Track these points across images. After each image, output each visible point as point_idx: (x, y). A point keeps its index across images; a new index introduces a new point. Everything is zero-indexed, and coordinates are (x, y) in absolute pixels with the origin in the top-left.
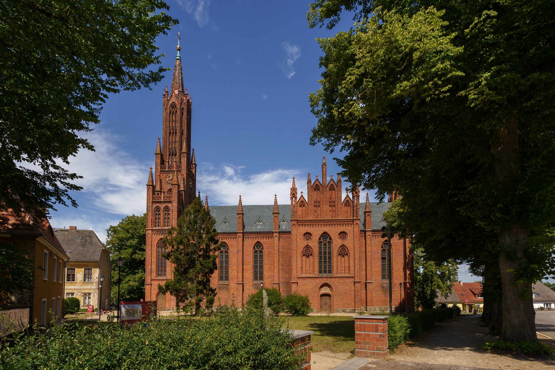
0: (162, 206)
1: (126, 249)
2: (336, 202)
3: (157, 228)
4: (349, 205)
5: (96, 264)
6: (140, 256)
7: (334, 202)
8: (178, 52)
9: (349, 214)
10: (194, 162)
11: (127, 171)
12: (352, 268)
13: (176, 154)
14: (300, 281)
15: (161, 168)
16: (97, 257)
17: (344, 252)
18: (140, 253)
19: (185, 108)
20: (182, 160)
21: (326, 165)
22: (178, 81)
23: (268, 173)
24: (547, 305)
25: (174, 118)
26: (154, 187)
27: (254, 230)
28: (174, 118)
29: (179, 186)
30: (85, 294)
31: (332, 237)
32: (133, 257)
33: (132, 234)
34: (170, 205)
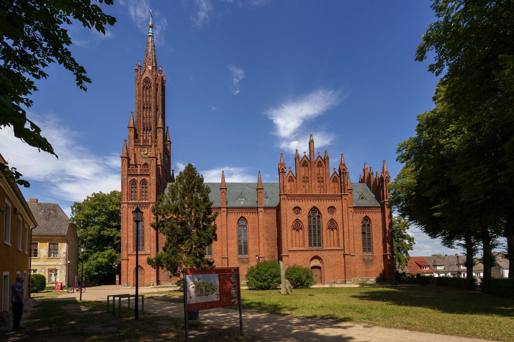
0: (139, 179)
1: (92, 226)
2: (324, 178)
3: (134, 201)
4: (337, 182)
5: (63, 239)
6: (109, 233)
7: (322, 178)
8: (151, 29)
9: (336, 190)
10: (168, 140)
11: (84, 164)
12: (341, 241)
13: (151, 129)
14: (291, 254)
15: (135, 142)
16: (64, 231)
17: (333, 226)
18: (109, 229)
19: (160, 84)
20: (158, 135)
21: (313, 143)
22: (151, 57)
23: (217, 169)
24: (477, 274)
25: (148, 93)
26: (129, 160)
27: (237, 206)
28: (148, 93)
29: (157, 159)
30: (50, 270)
31: (321, 211)
32: (102, 233)
33: (99, 210)
34: (147, 178)
